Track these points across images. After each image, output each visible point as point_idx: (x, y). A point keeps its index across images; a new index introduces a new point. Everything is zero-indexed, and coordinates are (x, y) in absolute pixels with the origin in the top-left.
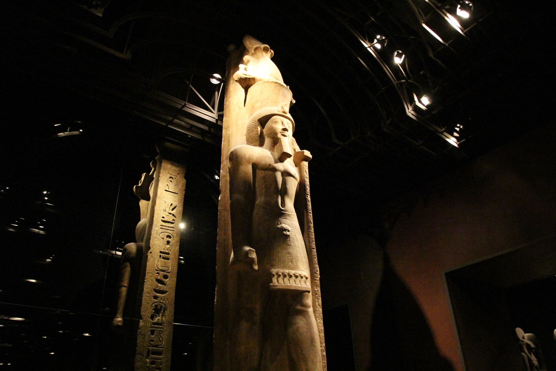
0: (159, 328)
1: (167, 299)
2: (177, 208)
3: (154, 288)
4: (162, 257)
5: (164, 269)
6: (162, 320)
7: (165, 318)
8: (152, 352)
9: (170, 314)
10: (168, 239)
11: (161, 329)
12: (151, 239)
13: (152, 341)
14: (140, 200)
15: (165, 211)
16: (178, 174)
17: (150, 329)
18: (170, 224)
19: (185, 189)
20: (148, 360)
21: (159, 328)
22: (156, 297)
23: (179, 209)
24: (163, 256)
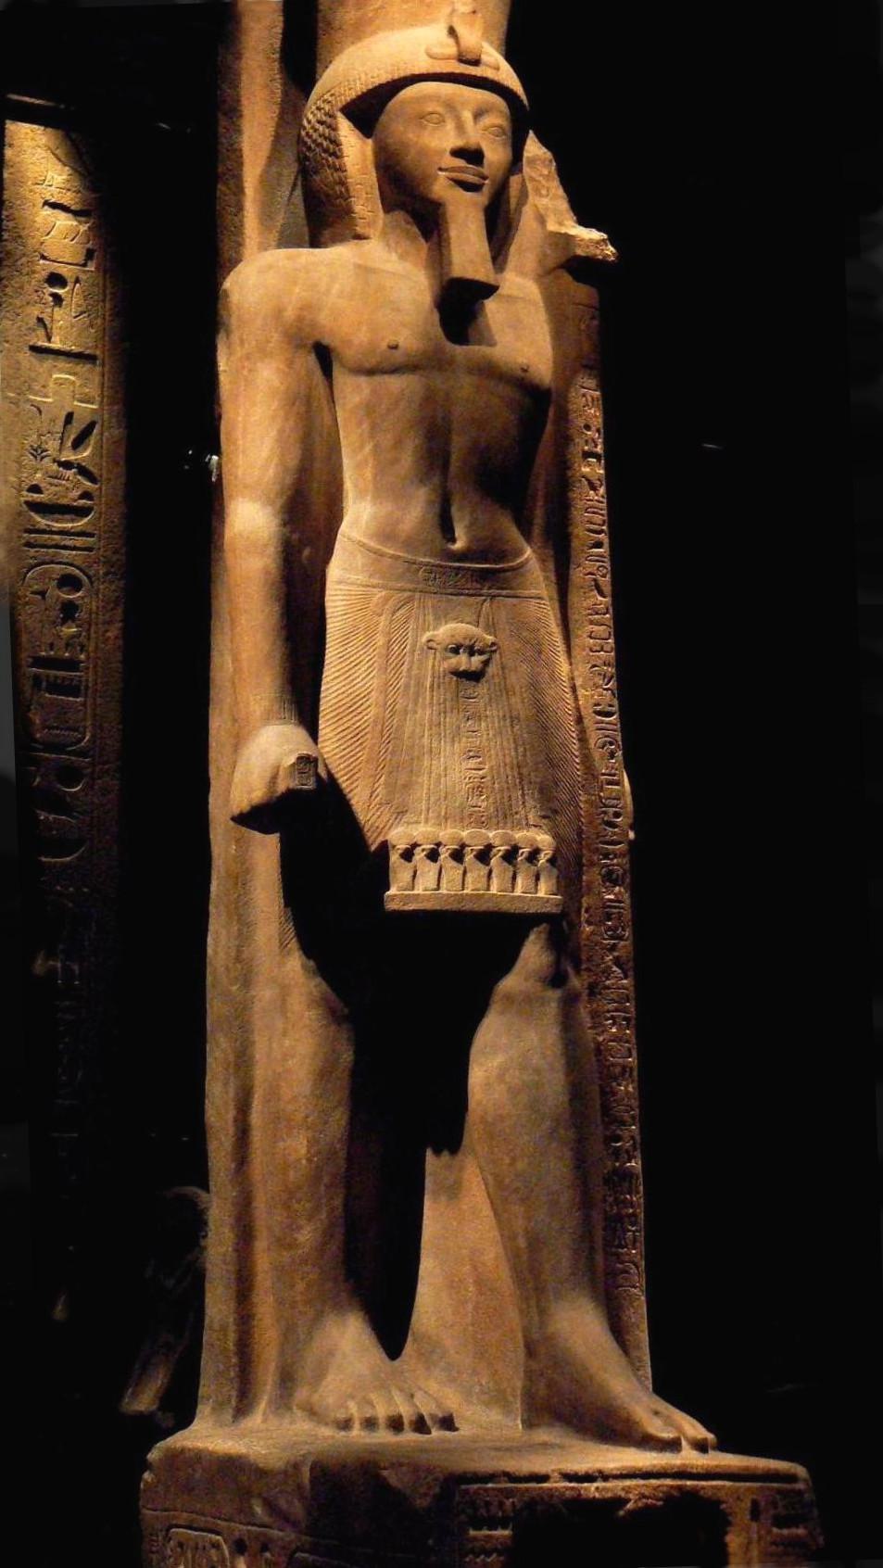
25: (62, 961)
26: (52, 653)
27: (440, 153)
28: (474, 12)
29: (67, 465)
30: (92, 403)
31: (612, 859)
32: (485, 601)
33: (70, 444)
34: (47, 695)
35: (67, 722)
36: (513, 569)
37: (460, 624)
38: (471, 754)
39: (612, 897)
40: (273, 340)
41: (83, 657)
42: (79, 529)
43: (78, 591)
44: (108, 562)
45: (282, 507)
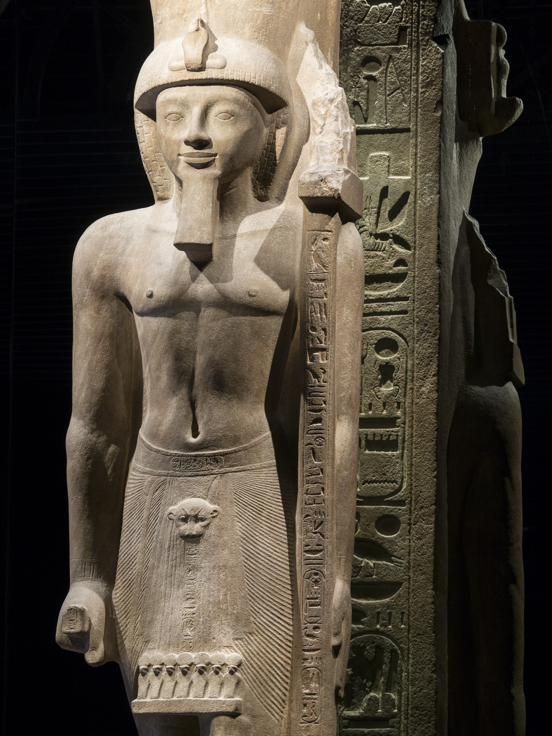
1: (403, 613)
2: (411, 198)
5: (376, 493)
7: (400, 693)
24: (370, 437)
25: (382, 692)
26: (370, 413)
27: (178, 144)
28: (197, 30)
29: (384, 236)
30: (407, 174)
31: (310, 663)
32: (215, 478)
33: (387, 216)
34: (367, 452)
35: (384, 474)
36: (256, 445)
37: (193, 499)
38: (188, 596)
39: (307, 691)
40: (87, 294)
41: (399, 413)
42: (393, 296)
43: (395, 353)
44: (422, 322)
45: (90, 419)
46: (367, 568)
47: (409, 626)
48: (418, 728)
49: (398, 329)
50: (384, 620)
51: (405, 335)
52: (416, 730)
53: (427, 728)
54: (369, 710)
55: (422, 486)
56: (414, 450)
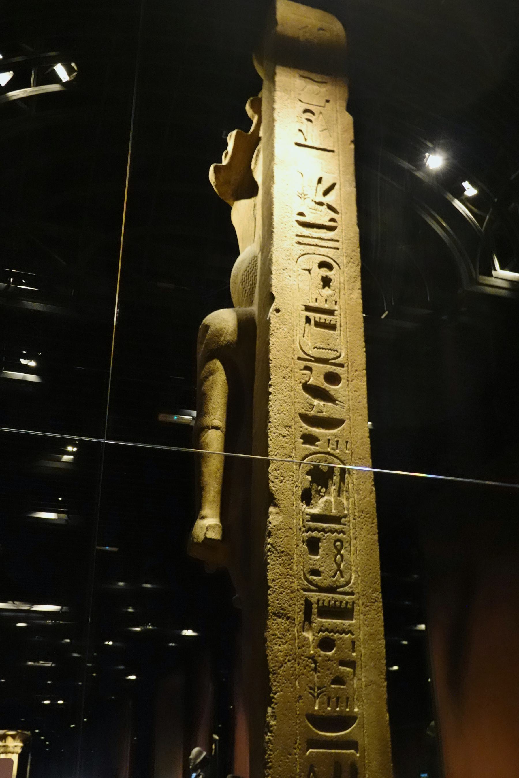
0: (332, 531)
1: (347, 442)
2: (337, 187)
3: (303, 411)
4: (312, 322)
5: (323, 356)
6: (339, 504)
7: (348, 499)
8: (318, 608)
9: (361, 487)
10: (324, 272)
11: (339, 533)
12: (273, 272)
13: (316, 572)
14: (229, 208)
15: (302, 196)
16: (327, 101)
17: (311, 567)
18: (325, 231)
19: (352, 138)
20: (309, 635)
21: (332, 531)
22: (309, 439)
23: (343, 189)
24: (317, 319)
46: (319, 406)
47: (352, 453)
48: (364, 527)
49: (333, 257)
50: (333, 445)
51: (338, 262)
52: (362, 528)
53: (371, 527)
54: (326, 510)
55: (356, 356)
56: (348, 333)
